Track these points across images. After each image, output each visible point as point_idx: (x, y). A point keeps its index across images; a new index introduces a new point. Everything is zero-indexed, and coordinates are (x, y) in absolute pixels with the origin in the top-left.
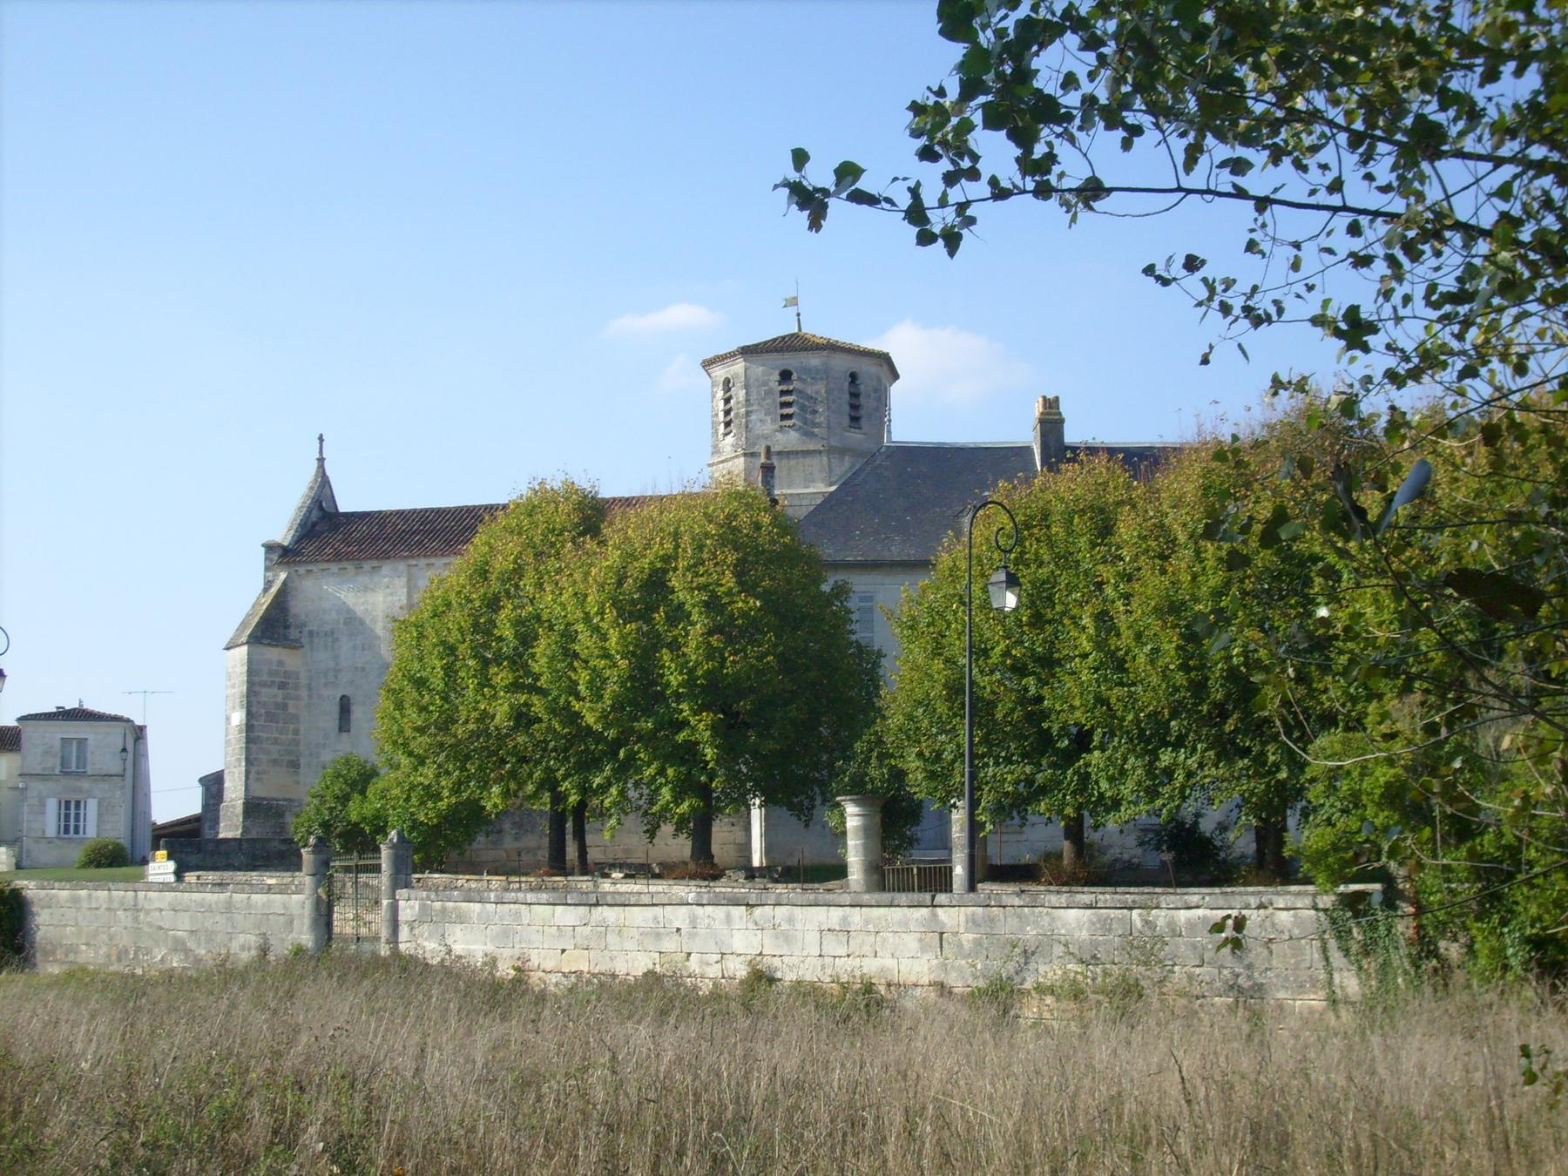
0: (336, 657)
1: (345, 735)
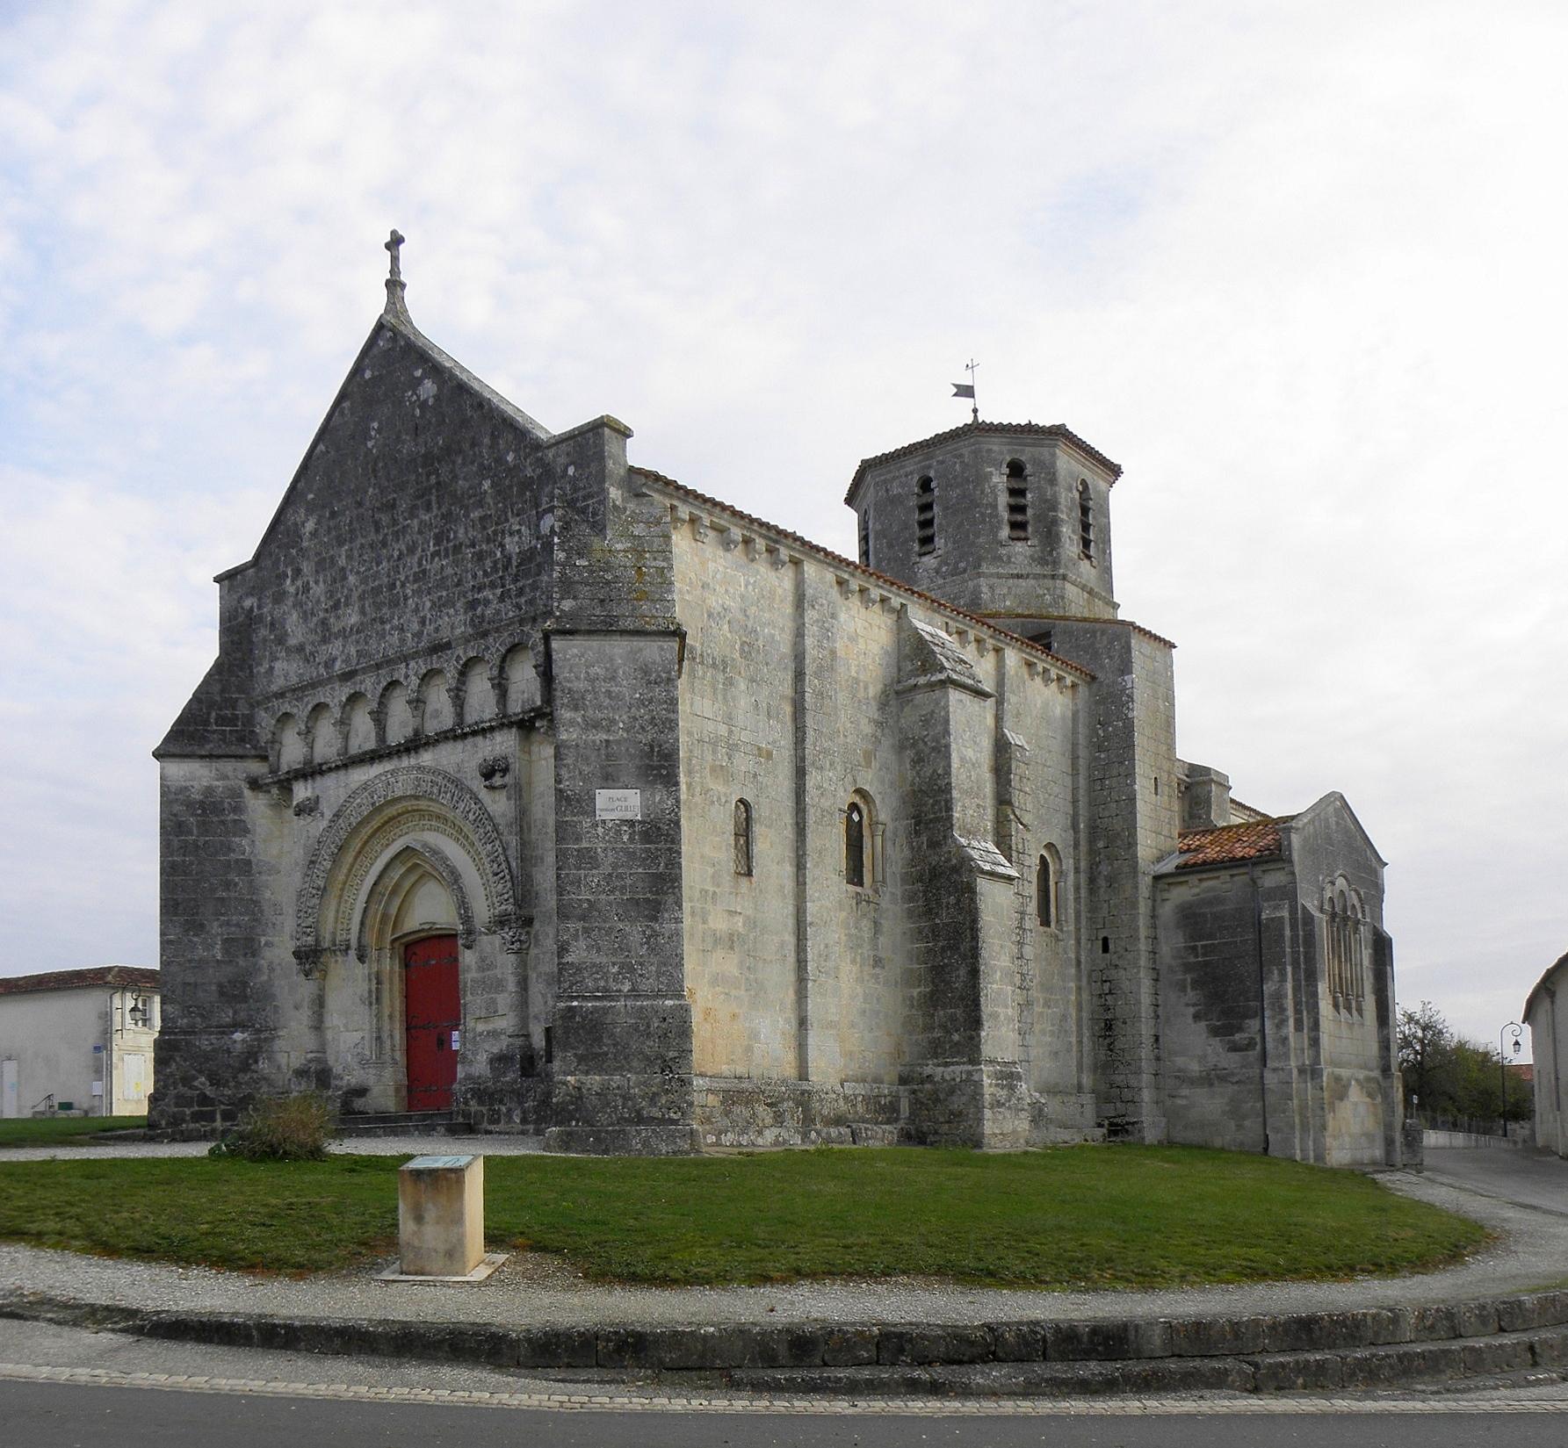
0: (729, 719)
1: (744, 881)
